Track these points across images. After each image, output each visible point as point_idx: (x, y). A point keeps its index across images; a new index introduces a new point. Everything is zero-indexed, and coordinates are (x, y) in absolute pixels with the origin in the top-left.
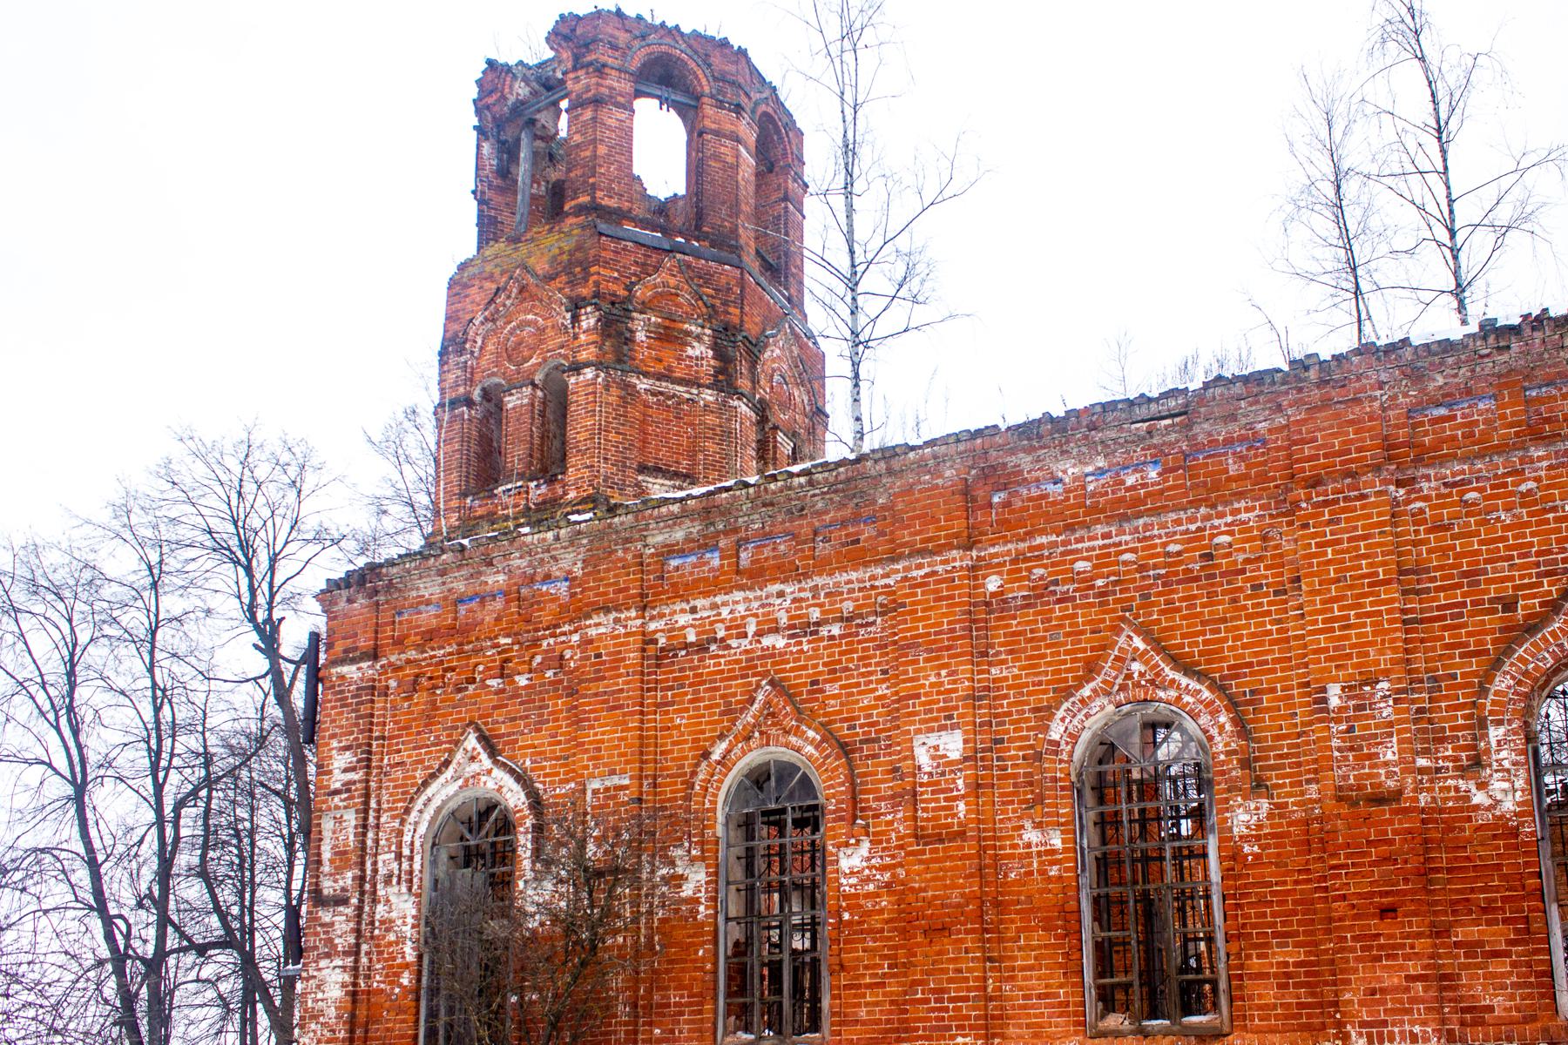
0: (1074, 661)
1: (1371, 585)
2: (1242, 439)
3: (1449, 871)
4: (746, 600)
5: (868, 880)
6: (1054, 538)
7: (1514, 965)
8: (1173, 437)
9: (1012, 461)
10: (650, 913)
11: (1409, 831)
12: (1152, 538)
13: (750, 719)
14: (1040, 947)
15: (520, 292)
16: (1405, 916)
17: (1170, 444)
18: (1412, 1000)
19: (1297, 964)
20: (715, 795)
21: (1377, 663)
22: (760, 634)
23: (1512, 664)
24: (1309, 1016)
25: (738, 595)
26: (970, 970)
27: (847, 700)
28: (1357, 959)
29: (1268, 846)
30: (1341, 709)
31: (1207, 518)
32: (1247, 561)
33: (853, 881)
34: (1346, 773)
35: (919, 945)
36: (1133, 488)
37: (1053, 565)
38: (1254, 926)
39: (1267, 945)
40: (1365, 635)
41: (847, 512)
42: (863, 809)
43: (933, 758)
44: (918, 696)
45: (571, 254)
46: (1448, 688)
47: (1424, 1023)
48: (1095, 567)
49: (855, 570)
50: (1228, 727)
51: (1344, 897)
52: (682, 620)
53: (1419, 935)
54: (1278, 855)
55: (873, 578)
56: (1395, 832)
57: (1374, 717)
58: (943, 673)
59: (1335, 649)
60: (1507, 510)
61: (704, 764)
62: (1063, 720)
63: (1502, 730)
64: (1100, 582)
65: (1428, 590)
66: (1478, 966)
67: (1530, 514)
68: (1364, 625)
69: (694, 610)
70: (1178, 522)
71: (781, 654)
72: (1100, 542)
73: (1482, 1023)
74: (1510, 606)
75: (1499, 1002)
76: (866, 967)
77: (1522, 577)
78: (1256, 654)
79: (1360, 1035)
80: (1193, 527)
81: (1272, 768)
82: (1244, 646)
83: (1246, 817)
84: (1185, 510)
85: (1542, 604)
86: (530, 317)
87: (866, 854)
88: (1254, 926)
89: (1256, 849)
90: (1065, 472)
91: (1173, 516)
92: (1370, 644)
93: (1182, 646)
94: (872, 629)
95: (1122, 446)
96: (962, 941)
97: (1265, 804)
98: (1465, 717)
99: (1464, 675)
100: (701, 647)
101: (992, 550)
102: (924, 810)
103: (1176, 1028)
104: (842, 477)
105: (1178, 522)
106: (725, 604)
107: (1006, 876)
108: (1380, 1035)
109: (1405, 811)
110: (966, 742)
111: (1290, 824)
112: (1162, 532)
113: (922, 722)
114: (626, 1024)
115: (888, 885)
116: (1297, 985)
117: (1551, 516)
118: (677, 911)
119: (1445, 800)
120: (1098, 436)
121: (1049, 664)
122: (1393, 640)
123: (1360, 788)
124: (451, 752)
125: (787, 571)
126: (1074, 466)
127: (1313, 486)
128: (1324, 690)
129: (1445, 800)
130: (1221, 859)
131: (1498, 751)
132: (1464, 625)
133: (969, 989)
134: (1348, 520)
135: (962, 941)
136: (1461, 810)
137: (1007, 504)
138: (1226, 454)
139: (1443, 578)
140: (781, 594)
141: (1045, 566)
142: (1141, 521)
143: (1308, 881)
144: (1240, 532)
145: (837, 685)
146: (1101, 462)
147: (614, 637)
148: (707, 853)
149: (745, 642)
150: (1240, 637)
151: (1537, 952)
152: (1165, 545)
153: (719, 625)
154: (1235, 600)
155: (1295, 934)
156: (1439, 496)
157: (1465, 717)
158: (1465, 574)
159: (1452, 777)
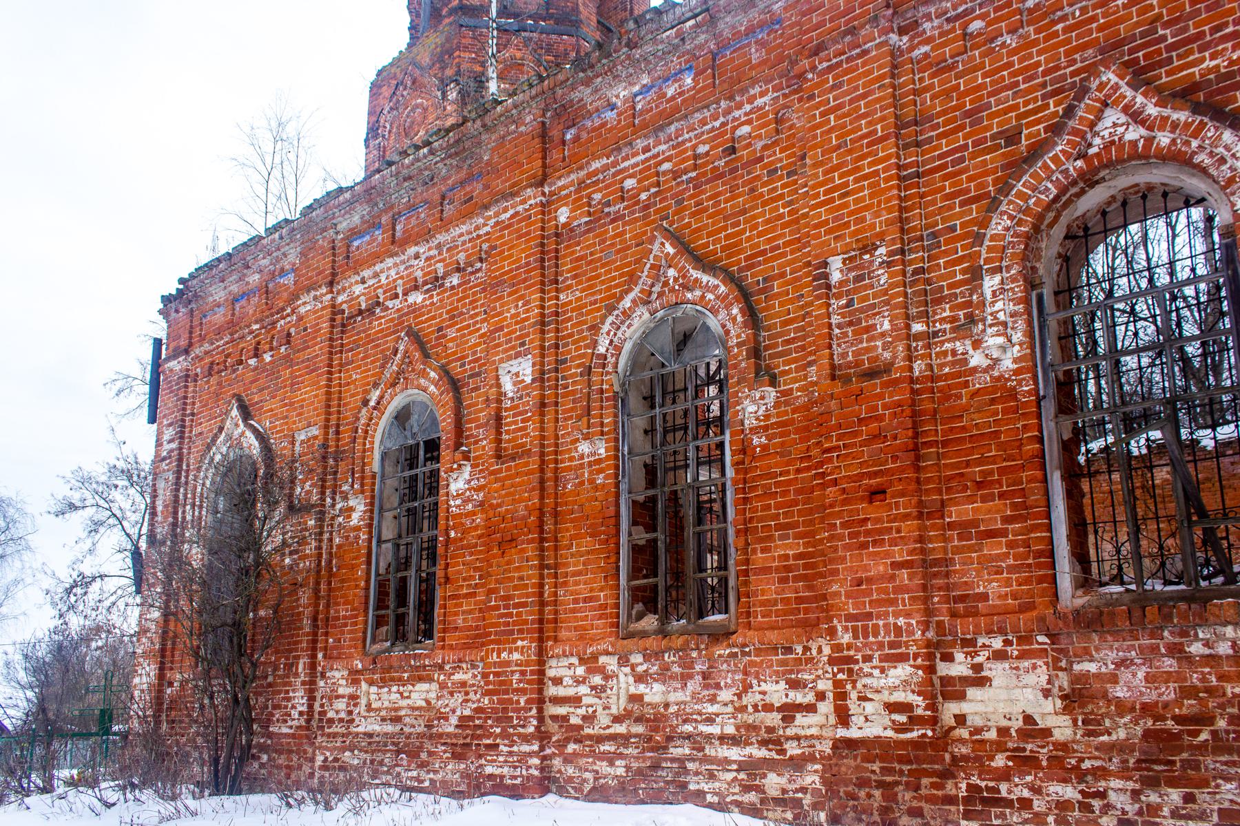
0: (621, 276)
1: (869, 145)
2: (762, 25)
3: (945, 444)
4: (396, 265)
5: (468, 500)
6: (605, 161)
7: (1011, 545)
8: (702, 38)
9: (575, 96)
10: (331, 540)
11: (899, 404)
12: (683, 142)
13: (395, 368)
14: (588, 552)
15: (414, 83)
16: (893, 497)
17: (700, 47)
18: (899, 590)
19: (798, 557)
20: (373, 437)
21: (873, 226)
22: (405, 294)
23: (1010, 202)
24: (806, 611)
25: (390, 262)
26: (529, 577)
27: (460, 341)
28: (847, 547)
29: (773, 436)
30: (841, 283)
31: (728, 112)
32: (765, 147)
33: (458, 502)
34: (844, 352)
35: (494, 557)
36: (673, 98)
37: (607, 187)
38: (761, 519)
39: (770, 538)
40: (862, 199)
41: (463, 174)
42: (468, 437)
43: (515, 384)
44: (501, 329)
45: (443, 46)
46: (947, 242)
47: (908, 615)
48: (639, 182)
49: (464, 223)
50: (739, 319)
51: (835, 482)
52: (358, 289)
53: (906, 517)
54: (783, 444)
55: (477, 228)
56: (885, 407)
57: (872, 287)
58: (520, 304)
59: (835, 219)
60: (1012, 31)
61: (364, 411)
62: (608, 333)
63: (997, 278)
64: (643, 196)
65: (930, 140)
66: (971, 549)
67: (1037, 31)
68: (862, 189)
69: (363, 282)
70: (703, 122)
71: (420, 309)
72: (642, 157)
73: (976, 614)
74: (1012, 138)
75: (993, 588)
76: (465, 579)
77: (1026, 103)
78: (769, 241)
79: (846, 629)
80: (717, 124)
81: (780, 354)
82: (760, 235)
83: (752, 408)
84: (707, 107)
85: (1046, 130)
86: (419, 101)
87: (467, 477)
88: (761, 519)
89: (763, 439)
90: (617, 96)
91: (698, 116)
92: (867, 208)
93: (707, 245)
94: (479, 275)
95: (661, 59)
96: (523, 550)
97: (771, 393)
98: (963, 272)
99: (963, 225)
100: (370, 311)
101: (560, 183)
102: (507, 432)
103: (691, 627)
104: (452, 141)
105: (703, 122)
106: (382, 271)
107: (565, 487)
108: (865, 628)
109: (895, 382)
110: (534, 365)
111: (794, 412)
112: (692, 134)
113: (506, 351)
114: (308, 634)
115: (482, 504)
116: (797, 579)
117: (1060, 26)
118: (347, 537)
119: (941, 366)
120: (637, 53)
121: (603, 283)
122: (889, 200)
123: (858, 364)
124: (223, 421)
125: (424, 235)
126: (625, 88)
127: (816, 54)
128: (825, 265)
129: (941, 366)
130: (734, 453)
131: (993, 303)
132: (966, 170)
133: (527, 596)
134: (850, 81)
135: (523, 550)
136: (959, 375)
137: (576, 139)
138: (749, 44)
139: (945, 124)
140: (417, 256)
141: (600, 190)
142: (673, 128)
143: (808, 469)
144: (758, 119)
145: (454, 329)
146: (645, 80)
147: (315, 312)
148: (365, 483)
149: (397, 302)
150: (755, 227)
151: (1034, 528)
152: (694, 147)
153: (380, 291)
154: (752, 190)
155: (795, 525)
156: (941, 35)
157: (963, 272)
158: (968, 114)
159: (949, 340)
